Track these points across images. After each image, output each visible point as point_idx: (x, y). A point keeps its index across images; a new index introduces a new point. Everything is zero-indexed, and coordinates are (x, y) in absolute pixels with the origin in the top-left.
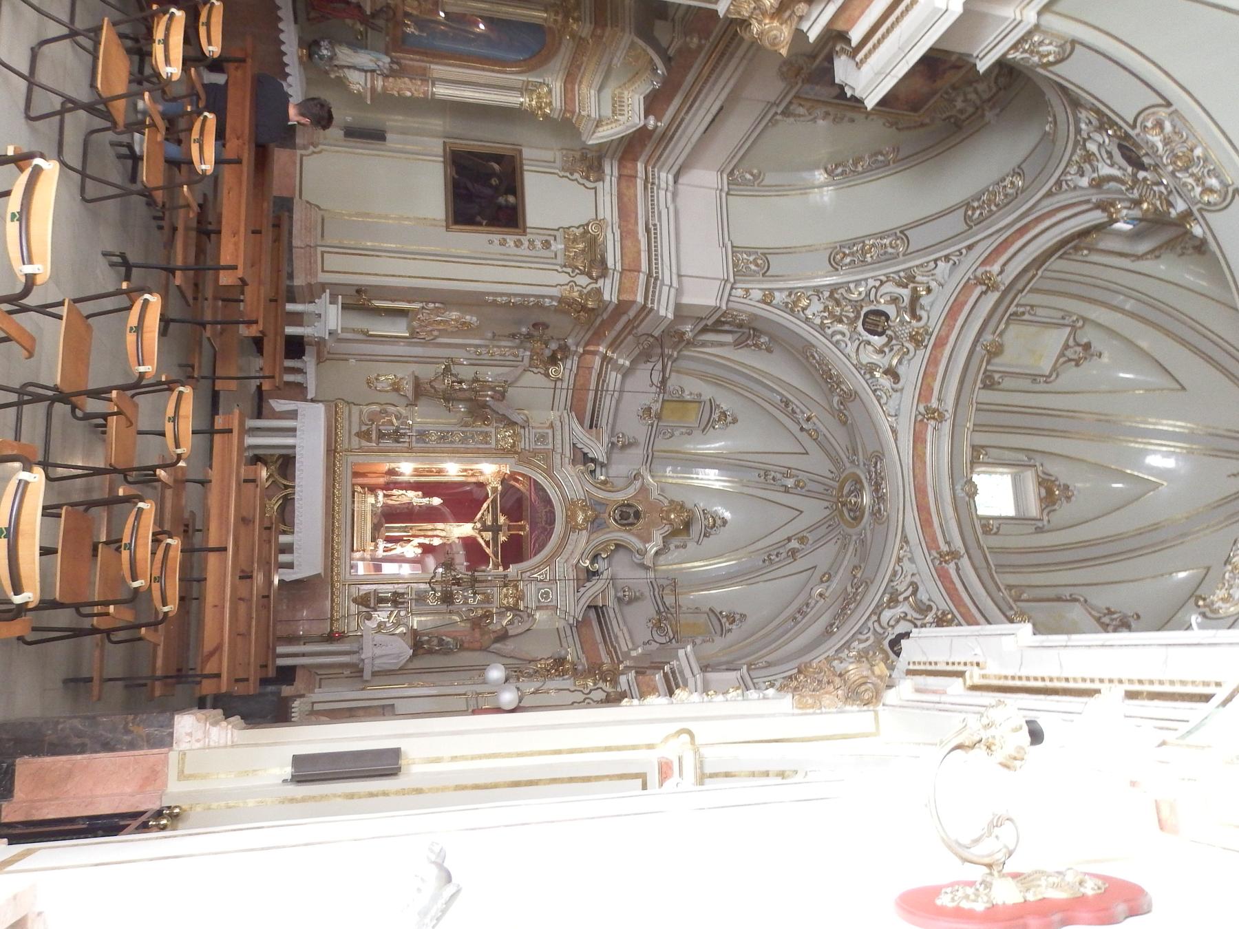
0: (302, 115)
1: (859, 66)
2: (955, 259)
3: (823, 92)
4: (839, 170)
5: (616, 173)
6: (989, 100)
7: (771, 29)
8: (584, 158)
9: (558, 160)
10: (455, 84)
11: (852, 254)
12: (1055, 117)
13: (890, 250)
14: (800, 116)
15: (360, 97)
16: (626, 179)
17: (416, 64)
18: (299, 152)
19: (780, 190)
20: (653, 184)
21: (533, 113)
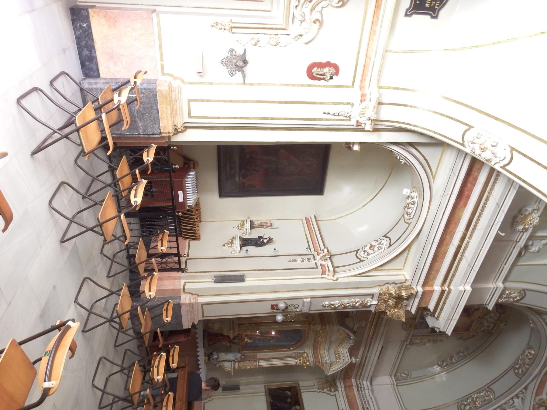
0: (207, 386)
1: (437, 319)
2: (521, 396)
3: (193, 331)
4: (445, 364)
5: (343, 386)
6: (498, 319)
7: (395, 313)
8: (327, 382)
9: (316, 385)
10: (268, 360)
11: (468, 404)
12: (532, 320)
13: (487, 398)
14: (417, 343)
15: (229, 372)
16: (348, 388)
17: (251, 354)
18: (203, 401)
19: (421, 379)
20: (361, 388)
21: (302, 366)
